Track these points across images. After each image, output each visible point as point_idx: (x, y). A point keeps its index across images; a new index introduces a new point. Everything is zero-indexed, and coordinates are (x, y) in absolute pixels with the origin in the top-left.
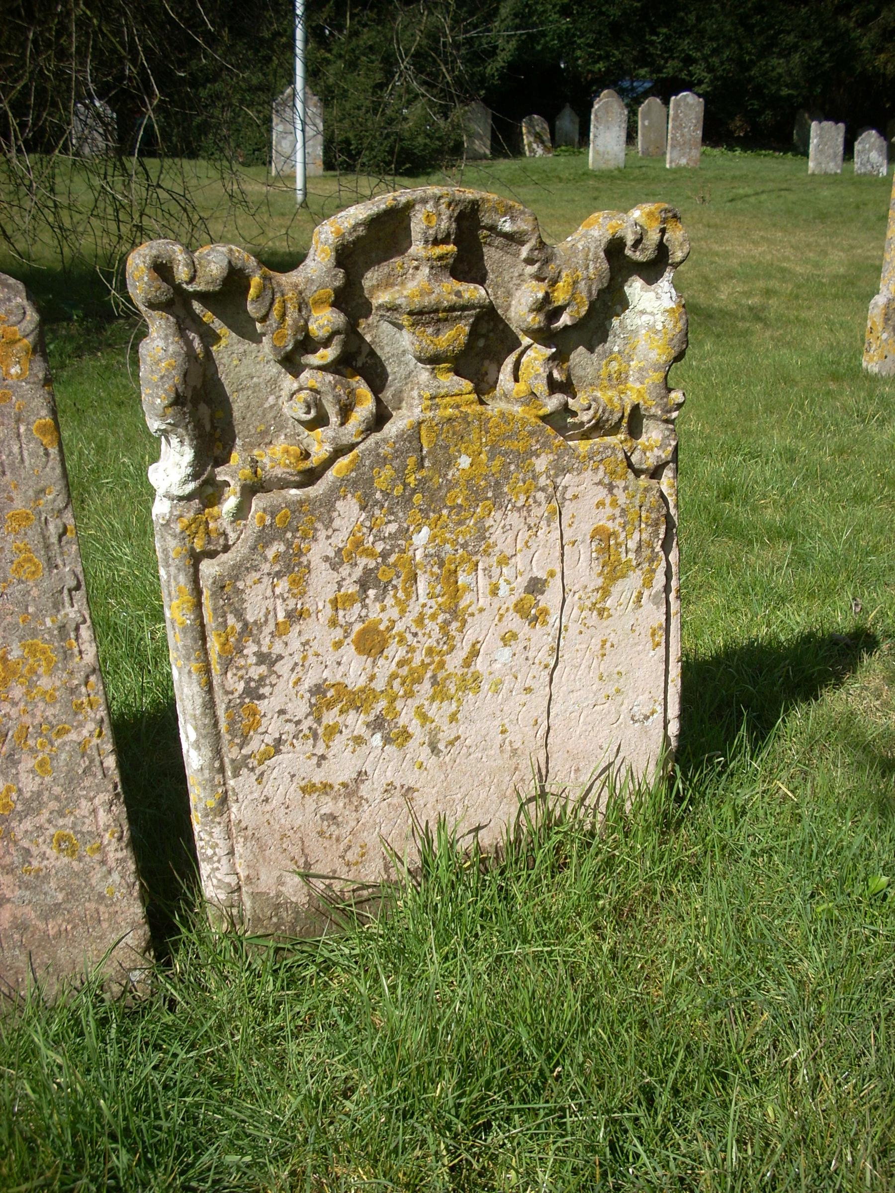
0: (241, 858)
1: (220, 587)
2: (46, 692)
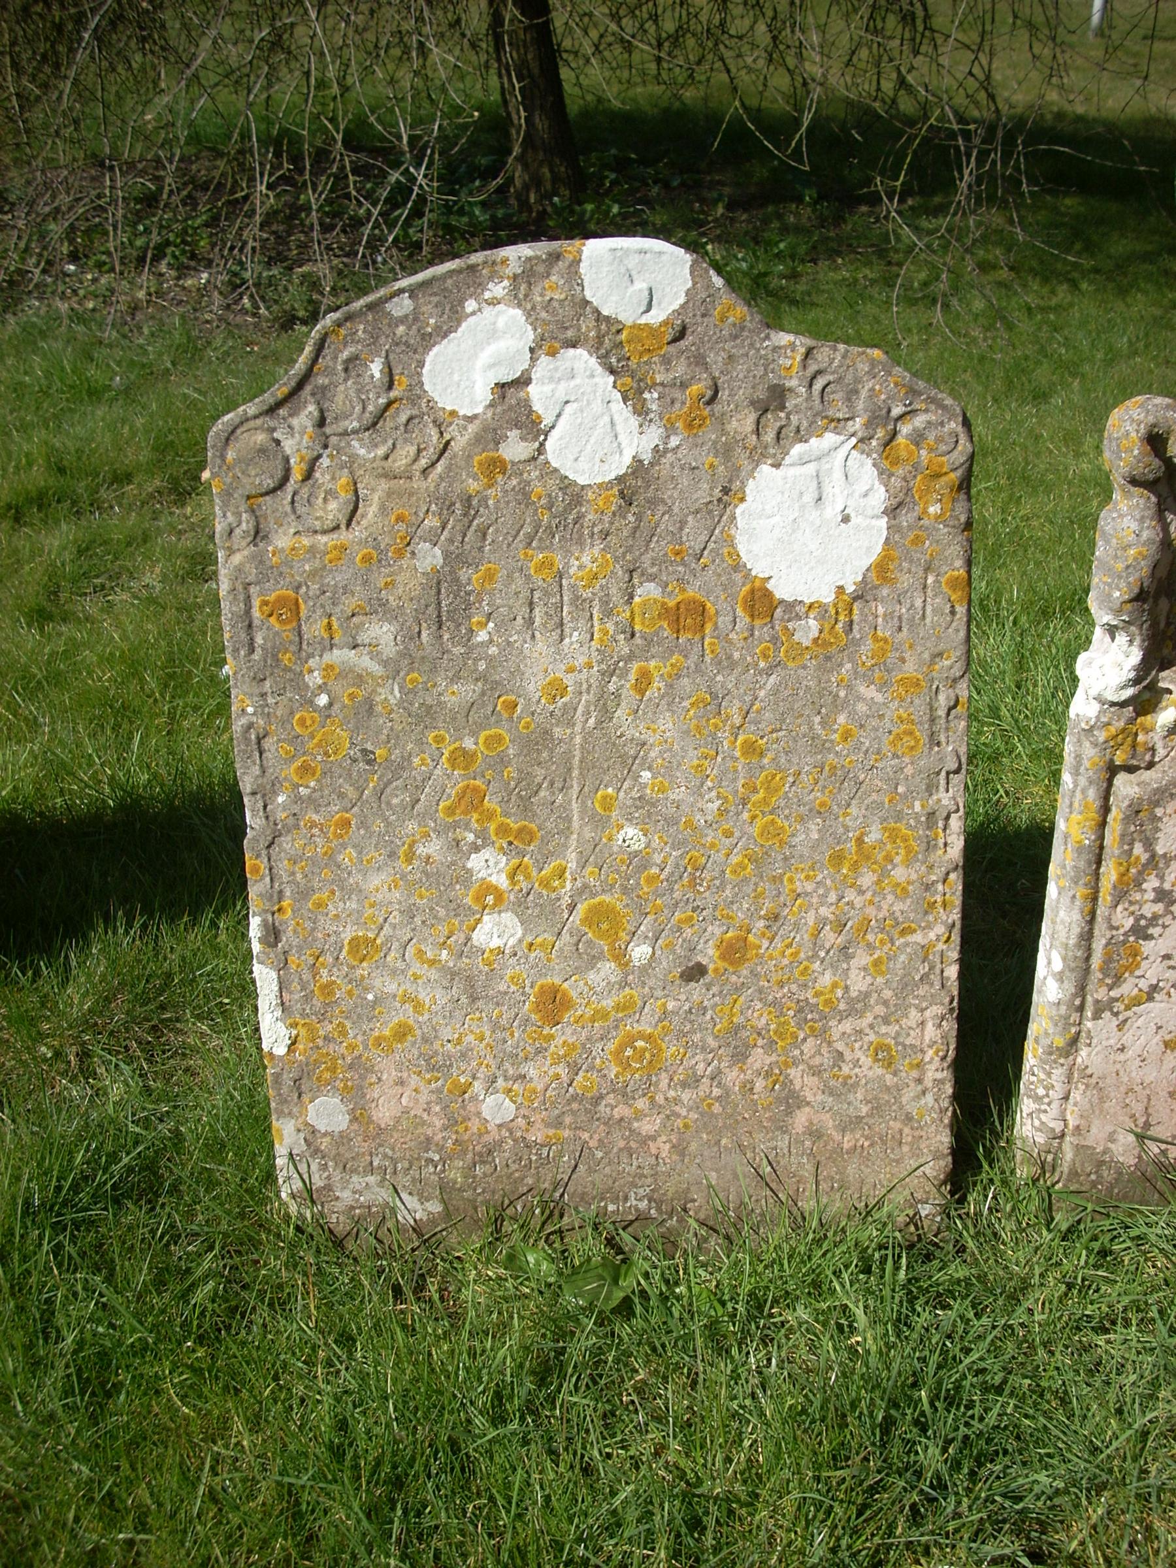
0: (1075, 1104)
1: (1135, 811)
2: (898, 884)
